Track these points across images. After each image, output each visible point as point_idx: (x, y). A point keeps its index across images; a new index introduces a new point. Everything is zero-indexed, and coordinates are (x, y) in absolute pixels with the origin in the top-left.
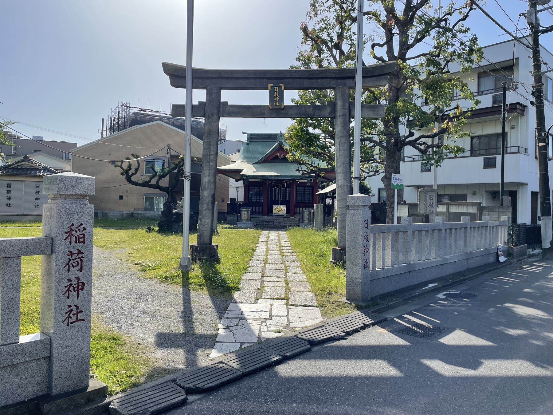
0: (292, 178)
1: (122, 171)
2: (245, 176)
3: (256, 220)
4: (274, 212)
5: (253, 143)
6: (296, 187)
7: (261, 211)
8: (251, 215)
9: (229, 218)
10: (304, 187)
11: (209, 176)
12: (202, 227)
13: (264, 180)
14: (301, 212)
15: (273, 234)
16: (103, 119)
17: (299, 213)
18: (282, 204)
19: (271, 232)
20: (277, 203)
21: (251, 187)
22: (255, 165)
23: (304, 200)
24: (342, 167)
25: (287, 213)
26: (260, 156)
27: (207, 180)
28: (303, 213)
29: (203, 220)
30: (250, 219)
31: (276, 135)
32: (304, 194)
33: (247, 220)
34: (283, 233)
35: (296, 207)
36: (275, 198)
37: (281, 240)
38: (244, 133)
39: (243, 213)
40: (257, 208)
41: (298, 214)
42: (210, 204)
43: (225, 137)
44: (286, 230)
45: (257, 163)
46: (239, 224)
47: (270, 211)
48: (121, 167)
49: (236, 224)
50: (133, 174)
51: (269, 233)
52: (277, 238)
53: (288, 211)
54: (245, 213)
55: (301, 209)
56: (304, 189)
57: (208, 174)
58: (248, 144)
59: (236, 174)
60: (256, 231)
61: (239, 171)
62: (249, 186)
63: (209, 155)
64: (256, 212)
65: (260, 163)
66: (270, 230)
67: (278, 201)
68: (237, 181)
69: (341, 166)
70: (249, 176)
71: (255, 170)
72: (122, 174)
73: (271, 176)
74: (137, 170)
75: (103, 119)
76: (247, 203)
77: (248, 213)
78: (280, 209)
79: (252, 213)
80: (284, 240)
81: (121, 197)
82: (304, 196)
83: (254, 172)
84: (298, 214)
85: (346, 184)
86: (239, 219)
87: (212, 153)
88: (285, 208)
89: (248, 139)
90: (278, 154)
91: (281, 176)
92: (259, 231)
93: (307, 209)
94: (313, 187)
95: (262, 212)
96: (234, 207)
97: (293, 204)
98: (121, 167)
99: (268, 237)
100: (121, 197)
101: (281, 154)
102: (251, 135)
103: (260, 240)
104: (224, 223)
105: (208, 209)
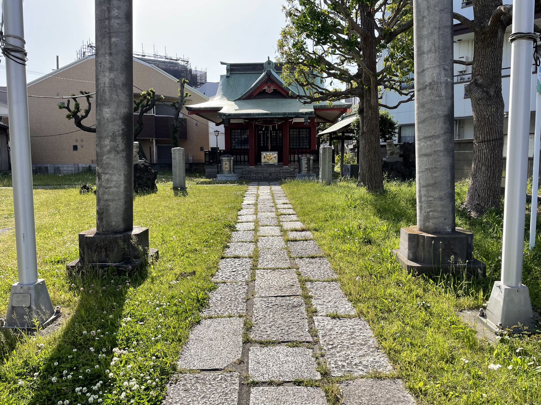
0: (285, 116)
1: (68, 113)
2: (224, 115)
3: (240, 171)
4: (263, 160)
5: (234, 76)
6: (290, 129)
7: (246, 159)
8: (234, 165)
9: (208, 170)
10: (299, 128)
11: (111, 69)
12: (104, 193)
13: (250, 119)
14: (296, 159)
15: (264, 191)
16: (57, 57)
17: (294, 161)
18: (272, 150)
19: (261, 187)
20: (267, 150)
21: (233, 131)
22: (237, 102)
23: (299, 145)
24: (435, 37)
26: (243, 91)
27: (107, 80)
28: (299, 161)
29: (104, 177)
30: (233, 170)
31: (261, 65)
33: (230, 172)
34: (277, 188)
35: (290, 153)
36: (264, 144)
37: (277, 201)
38: (222, 63)
39: (224, 163)
40: (242, 157)
41: (292, 163)
42: (119, 140)
43: (206, 80)
44: (280, 184)
45: (239, 99)
46: (220, 177)
47: (258, 159)
48: (68, 108)
49: (216, 177)
50: (83, 117)
51: (258, 189)
52: (270, 197)
53: (280, 159)
54: (226, 163)
55: (296, 156)
56: (299, 132)
57: (108, 65)
58: (227, 77)
59: (213, 113)
60: (240, 186)
61: (215, 111)
63: (109, 19)
65: (244, 99)
66: (259, 185)
67: (267, 146)
68: (217, 125)
69: (432, 33)
70: (229, 115)
71: (237, 108)
72: (68, 117)
73: (259, 114)
74: (87, 112)
75: (57, 57)
76: (229, 151)
77: (230, 162)
78: (270, 157)
79: (236, 162)
80: (281, 201)
81: (75, 148)
82: (299, 140)
83: (236, 110)
84: (292, 163)
85: (443, 79)
86: (220, 171)
87: (115, 12)
89: (228, 70)
90: (266, 88)
91: (271, 114)
92: (244, 187)
93: (304, 155)
94: (310, 128)
95: (248, 161)
96: (214, 155)
98: (68, 108)
99: (257, 196)
100: (75, 148)
101: (269, 87)
102: (231, 65)
103: (245, 202)
104: (200, 176)
105: (114, 149)
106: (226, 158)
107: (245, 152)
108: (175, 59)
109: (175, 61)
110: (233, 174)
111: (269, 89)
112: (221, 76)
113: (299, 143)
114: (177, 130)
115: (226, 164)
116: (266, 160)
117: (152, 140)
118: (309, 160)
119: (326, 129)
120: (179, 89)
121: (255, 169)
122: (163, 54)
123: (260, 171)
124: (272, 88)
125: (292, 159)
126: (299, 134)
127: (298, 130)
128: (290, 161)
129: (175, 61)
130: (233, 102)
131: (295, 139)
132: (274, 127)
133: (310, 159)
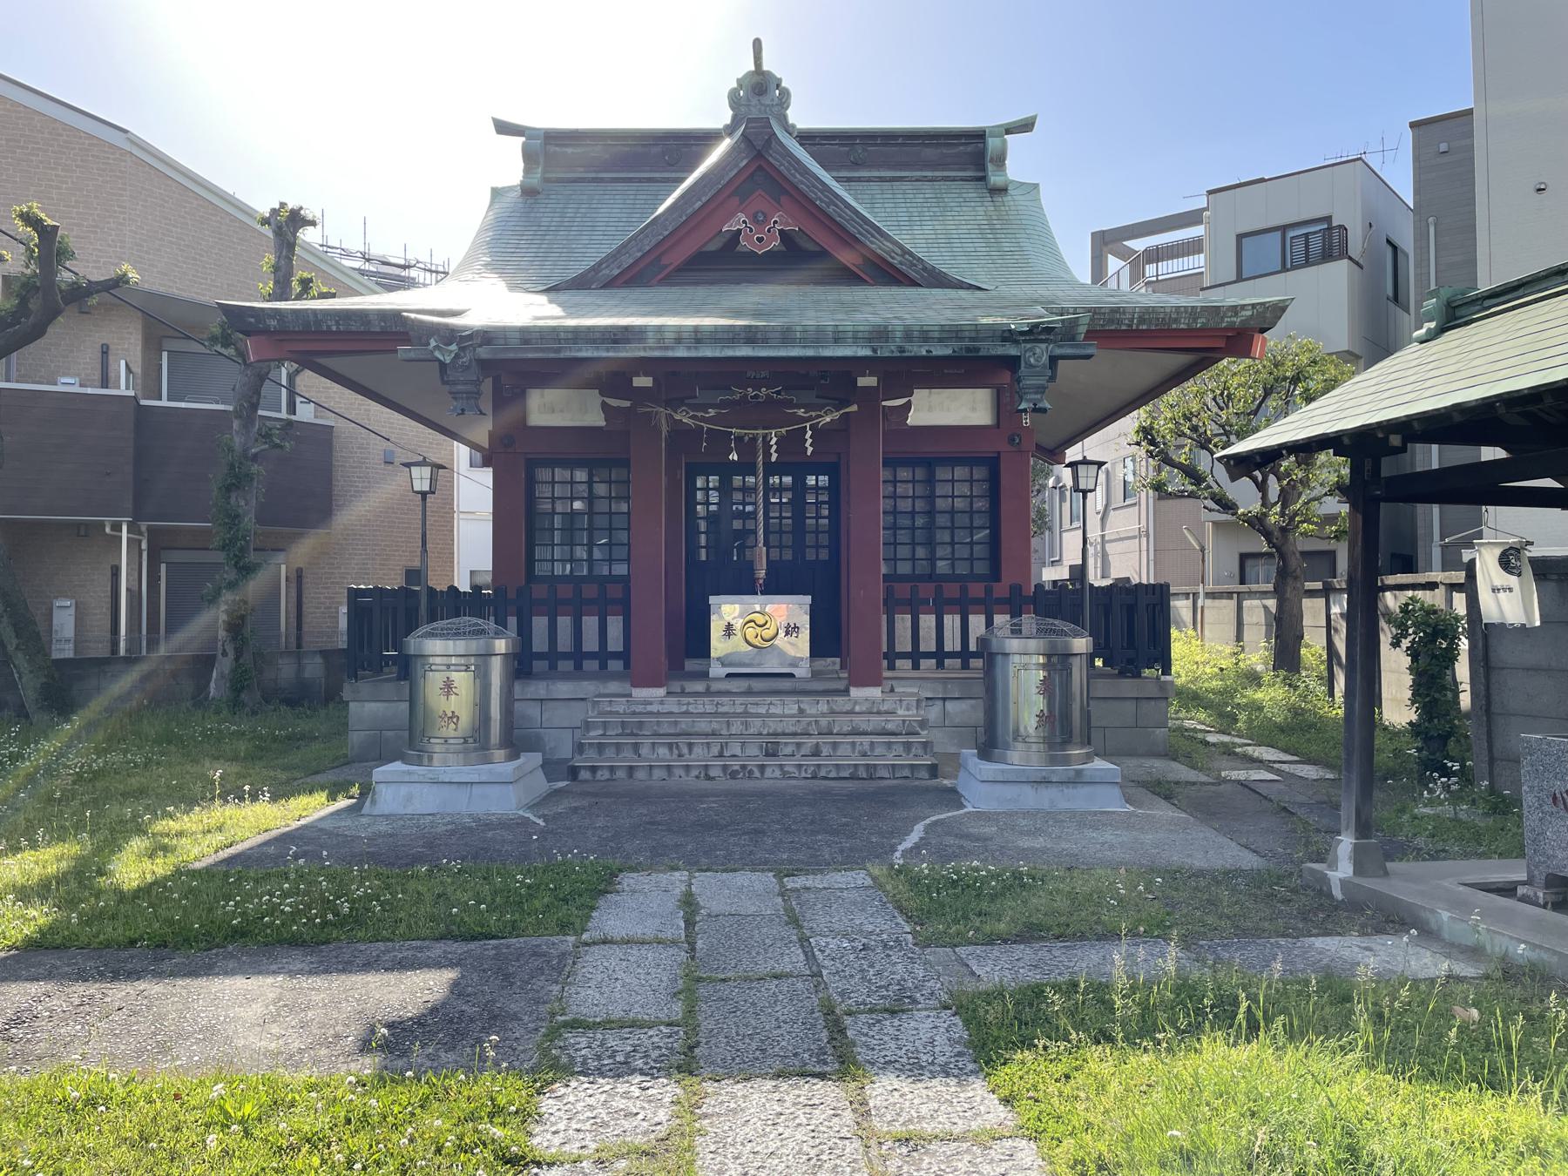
4: (719, 645)
7: (615, 643)
17: (916, 656)
18: (777, 585)
20: (742, 585)
23: (932, 560)
25: (817, 650)
32: (931, 513)
33: (477, 743)
35: (892, 606)
38: (503, 128)
39: (435, 680)
40: (590, 623)
56: (931, 481)
62: (532, 464)
64: (553, 656)
65: (610, 284)
67: (750, 567)
76: (508, 598)
82: (930, 527)
84: (904, 664)
88: (804, 621)
90: (738, 222)
94: (993, 465)
95: (625, 656)
97: (864, 588)
101: (758, 219)
106: (460, 646)
107: (611, 597)
108: (402, 262)
109: (397, 271)
110: (503, 767)
111: (756, 229)
112: (496, 193)
113: (931, 544)
114: (249, 477)
115: (448, 687)
116: (737, 645)
117: (117, 527)
118: (1058, 662)
119: (1256, 430)
120: (269, 259)
121: (672, 705)
122: (356, 245)
123: (703, 725)
124: (780, 220)
125: (903, 644)
126: (931, 498)
127: (920, 473)
128: (892, 656)
129: (397, 271)
130: (543, 299)
131: (962, 520)
132: (791, 442)
133: (1068, 656)
